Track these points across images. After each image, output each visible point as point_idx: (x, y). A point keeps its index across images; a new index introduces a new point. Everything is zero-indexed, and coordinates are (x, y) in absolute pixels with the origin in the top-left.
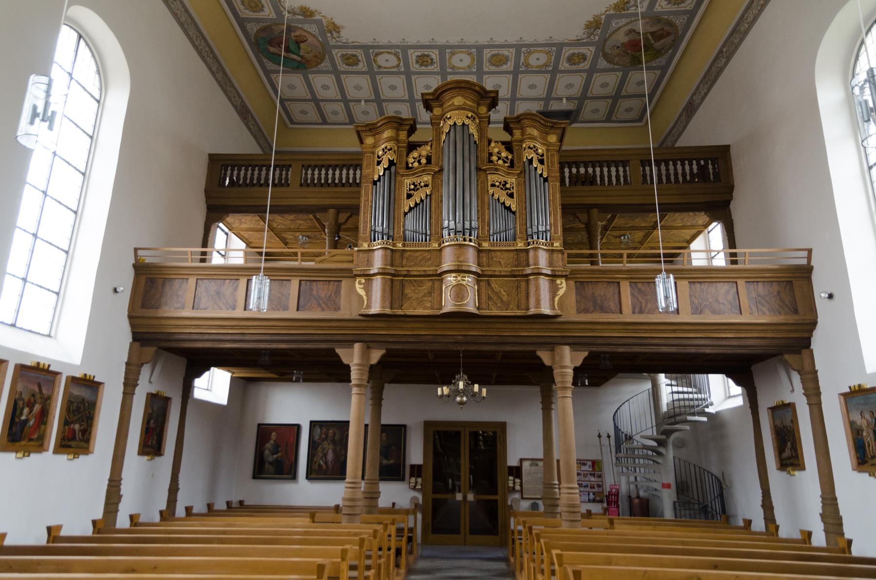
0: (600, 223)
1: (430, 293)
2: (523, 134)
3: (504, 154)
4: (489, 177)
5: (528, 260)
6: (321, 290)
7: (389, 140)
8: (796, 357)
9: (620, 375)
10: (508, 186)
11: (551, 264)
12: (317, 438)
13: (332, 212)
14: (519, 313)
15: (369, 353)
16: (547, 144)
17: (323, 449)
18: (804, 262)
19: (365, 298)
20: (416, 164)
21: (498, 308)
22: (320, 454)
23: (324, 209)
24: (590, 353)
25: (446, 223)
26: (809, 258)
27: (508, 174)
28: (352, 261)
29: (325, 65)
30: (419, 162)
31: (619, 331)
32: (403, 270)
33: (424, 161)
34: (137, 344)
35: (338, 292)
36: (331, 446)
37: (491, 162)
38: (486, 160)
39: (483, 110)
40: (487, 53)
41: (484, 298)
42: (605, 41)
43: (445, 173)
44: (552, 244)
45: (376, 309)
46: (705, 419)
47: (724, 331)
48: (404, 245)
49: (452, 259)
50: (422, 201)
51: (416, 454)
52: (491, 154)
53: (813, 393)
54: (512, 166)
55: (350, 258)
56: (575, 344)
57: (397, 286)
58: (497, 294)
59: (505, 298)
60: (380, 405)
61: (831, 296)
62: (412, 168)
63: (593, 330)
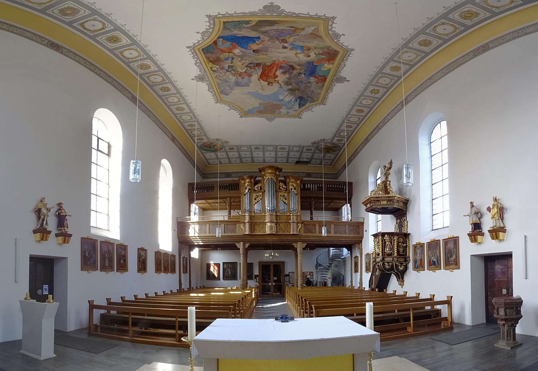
0: (313, 203)
1: (262, 228)
2: (290, 180)
3: (284, 187)
4: (279, 193)
5: (290, 218)
6: (230, 227)
7: (249, 182)
8: (359, 245)
9: (317, 248)
10: (285, 196)
11: (297, 219)
12: (225, 267)
13: (228, 198)
14: (288, 233)
15: (245, 245)
16: (297, 184)
17: (227, 270)
18: (363, 221)
19: (244, 229)
20: (257, 189)
21: (282, 232)
22: (226, 272)
23: (226, 198)
24: (307, 244)
25: (267, 208)
26: (364, 220)
27: (285, 193)
28: (239, 218)
29: (223, 150)
30: (258, 188)
31: (315, 238)
32: (254, 221)
33: (259, 188)
34: (180, 244)
35: (235, 227)
36: (230, 270)
37: (280, 189)
38: (278, 188)
39: (277, 173)
40: (279, 147)
41: (278, 229)
42: (318, 147)
43: (266, 192)
44: (297, 214)
45: (247, 233)
46: (340, 260)
47: (342, 238)
48: (254, 214)
49: (269, 218)
50: (259, 201)
51: (256, 272)
52: (280, 186)
53: (361, 254)
54: (286, 190)
55: (239, 217)
56: (303, 241)
57: (253, 226)
58: (282, 228)
59: (284, 229)
60: (247, 258)
61: (366, 231)
62: (256, 190)
63: (308, 238)
